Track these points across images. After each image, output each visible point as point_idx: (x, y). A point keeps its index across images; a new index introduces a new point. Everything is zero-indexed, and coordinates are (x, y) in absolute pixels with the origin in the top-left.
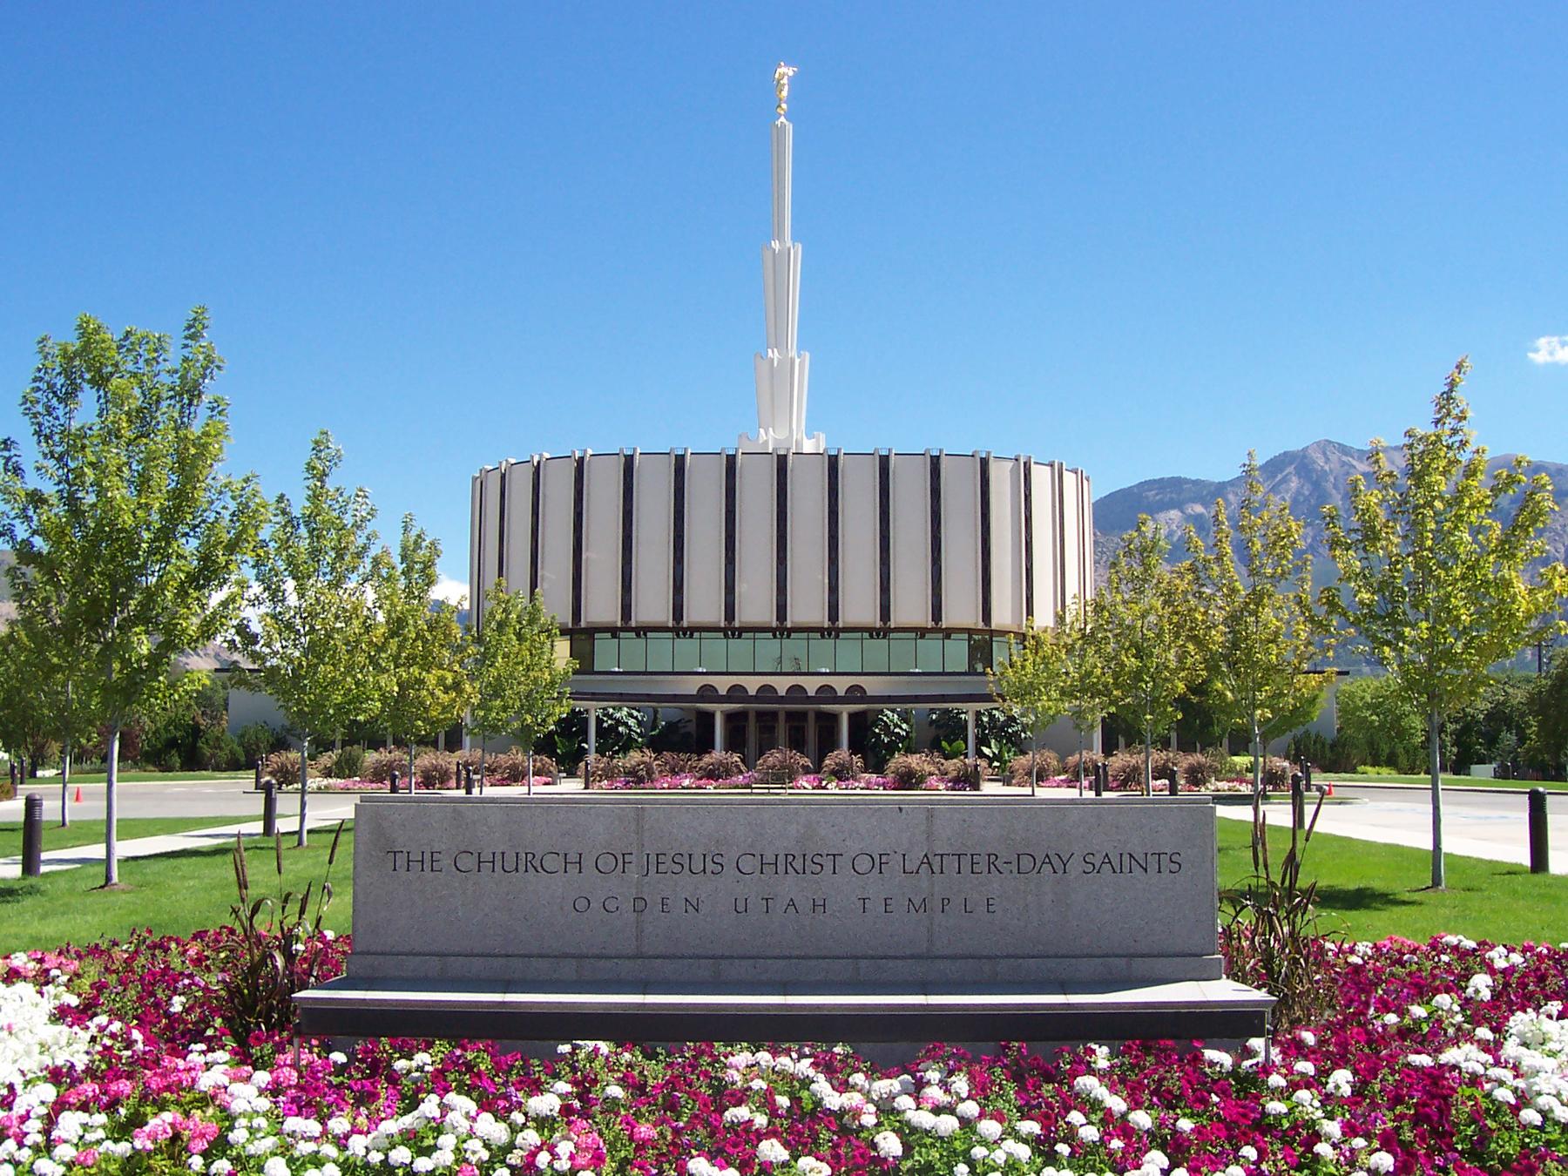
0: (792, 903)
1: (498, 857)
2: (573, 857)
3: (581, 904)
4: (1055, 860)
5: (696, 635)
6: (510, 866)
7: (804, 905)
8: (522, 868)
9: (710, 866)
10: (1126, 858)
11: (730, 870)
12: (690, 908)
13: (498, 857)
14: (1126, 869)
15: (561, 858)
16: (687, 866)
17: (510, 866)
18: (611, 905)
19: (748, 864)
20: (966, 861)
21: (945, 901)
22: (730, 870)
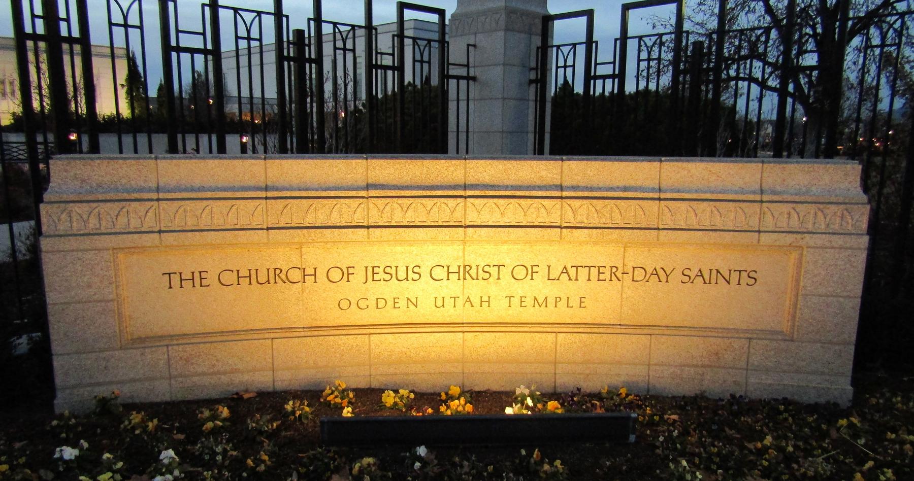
0: (469, 300)
1: (253, 273)
2: (310, 271)
3: (344, 304)
4: (661, 273)
5: (257, 83)
6: (263, 279)
7: (476, 301)
8: (272, 280)
9: (493, 271)
10: (714, 272)
11: (425, 277)
12: (414, 301)
13: (253, 273)
14: (713, 281)
15: (235, 273)
16: (394, 276)
17: (263, 279)
18: (362, 304)
19: (439, 273)
20: (594, 271)
21: (558, 299)
22: (425, 277)
